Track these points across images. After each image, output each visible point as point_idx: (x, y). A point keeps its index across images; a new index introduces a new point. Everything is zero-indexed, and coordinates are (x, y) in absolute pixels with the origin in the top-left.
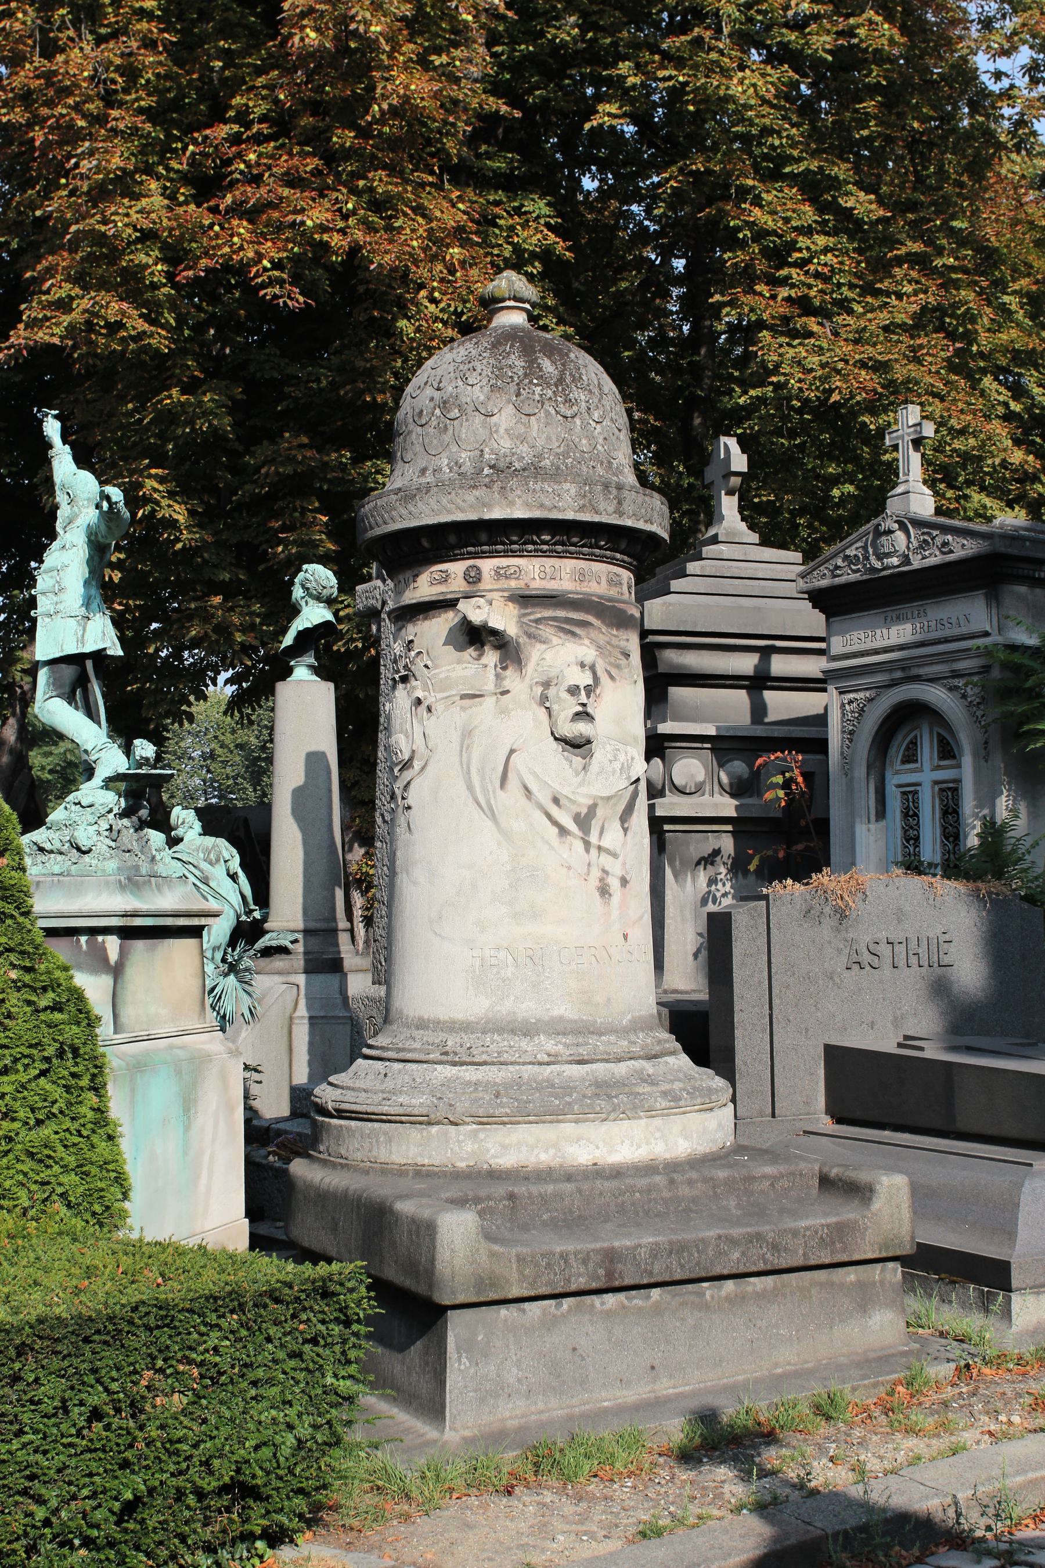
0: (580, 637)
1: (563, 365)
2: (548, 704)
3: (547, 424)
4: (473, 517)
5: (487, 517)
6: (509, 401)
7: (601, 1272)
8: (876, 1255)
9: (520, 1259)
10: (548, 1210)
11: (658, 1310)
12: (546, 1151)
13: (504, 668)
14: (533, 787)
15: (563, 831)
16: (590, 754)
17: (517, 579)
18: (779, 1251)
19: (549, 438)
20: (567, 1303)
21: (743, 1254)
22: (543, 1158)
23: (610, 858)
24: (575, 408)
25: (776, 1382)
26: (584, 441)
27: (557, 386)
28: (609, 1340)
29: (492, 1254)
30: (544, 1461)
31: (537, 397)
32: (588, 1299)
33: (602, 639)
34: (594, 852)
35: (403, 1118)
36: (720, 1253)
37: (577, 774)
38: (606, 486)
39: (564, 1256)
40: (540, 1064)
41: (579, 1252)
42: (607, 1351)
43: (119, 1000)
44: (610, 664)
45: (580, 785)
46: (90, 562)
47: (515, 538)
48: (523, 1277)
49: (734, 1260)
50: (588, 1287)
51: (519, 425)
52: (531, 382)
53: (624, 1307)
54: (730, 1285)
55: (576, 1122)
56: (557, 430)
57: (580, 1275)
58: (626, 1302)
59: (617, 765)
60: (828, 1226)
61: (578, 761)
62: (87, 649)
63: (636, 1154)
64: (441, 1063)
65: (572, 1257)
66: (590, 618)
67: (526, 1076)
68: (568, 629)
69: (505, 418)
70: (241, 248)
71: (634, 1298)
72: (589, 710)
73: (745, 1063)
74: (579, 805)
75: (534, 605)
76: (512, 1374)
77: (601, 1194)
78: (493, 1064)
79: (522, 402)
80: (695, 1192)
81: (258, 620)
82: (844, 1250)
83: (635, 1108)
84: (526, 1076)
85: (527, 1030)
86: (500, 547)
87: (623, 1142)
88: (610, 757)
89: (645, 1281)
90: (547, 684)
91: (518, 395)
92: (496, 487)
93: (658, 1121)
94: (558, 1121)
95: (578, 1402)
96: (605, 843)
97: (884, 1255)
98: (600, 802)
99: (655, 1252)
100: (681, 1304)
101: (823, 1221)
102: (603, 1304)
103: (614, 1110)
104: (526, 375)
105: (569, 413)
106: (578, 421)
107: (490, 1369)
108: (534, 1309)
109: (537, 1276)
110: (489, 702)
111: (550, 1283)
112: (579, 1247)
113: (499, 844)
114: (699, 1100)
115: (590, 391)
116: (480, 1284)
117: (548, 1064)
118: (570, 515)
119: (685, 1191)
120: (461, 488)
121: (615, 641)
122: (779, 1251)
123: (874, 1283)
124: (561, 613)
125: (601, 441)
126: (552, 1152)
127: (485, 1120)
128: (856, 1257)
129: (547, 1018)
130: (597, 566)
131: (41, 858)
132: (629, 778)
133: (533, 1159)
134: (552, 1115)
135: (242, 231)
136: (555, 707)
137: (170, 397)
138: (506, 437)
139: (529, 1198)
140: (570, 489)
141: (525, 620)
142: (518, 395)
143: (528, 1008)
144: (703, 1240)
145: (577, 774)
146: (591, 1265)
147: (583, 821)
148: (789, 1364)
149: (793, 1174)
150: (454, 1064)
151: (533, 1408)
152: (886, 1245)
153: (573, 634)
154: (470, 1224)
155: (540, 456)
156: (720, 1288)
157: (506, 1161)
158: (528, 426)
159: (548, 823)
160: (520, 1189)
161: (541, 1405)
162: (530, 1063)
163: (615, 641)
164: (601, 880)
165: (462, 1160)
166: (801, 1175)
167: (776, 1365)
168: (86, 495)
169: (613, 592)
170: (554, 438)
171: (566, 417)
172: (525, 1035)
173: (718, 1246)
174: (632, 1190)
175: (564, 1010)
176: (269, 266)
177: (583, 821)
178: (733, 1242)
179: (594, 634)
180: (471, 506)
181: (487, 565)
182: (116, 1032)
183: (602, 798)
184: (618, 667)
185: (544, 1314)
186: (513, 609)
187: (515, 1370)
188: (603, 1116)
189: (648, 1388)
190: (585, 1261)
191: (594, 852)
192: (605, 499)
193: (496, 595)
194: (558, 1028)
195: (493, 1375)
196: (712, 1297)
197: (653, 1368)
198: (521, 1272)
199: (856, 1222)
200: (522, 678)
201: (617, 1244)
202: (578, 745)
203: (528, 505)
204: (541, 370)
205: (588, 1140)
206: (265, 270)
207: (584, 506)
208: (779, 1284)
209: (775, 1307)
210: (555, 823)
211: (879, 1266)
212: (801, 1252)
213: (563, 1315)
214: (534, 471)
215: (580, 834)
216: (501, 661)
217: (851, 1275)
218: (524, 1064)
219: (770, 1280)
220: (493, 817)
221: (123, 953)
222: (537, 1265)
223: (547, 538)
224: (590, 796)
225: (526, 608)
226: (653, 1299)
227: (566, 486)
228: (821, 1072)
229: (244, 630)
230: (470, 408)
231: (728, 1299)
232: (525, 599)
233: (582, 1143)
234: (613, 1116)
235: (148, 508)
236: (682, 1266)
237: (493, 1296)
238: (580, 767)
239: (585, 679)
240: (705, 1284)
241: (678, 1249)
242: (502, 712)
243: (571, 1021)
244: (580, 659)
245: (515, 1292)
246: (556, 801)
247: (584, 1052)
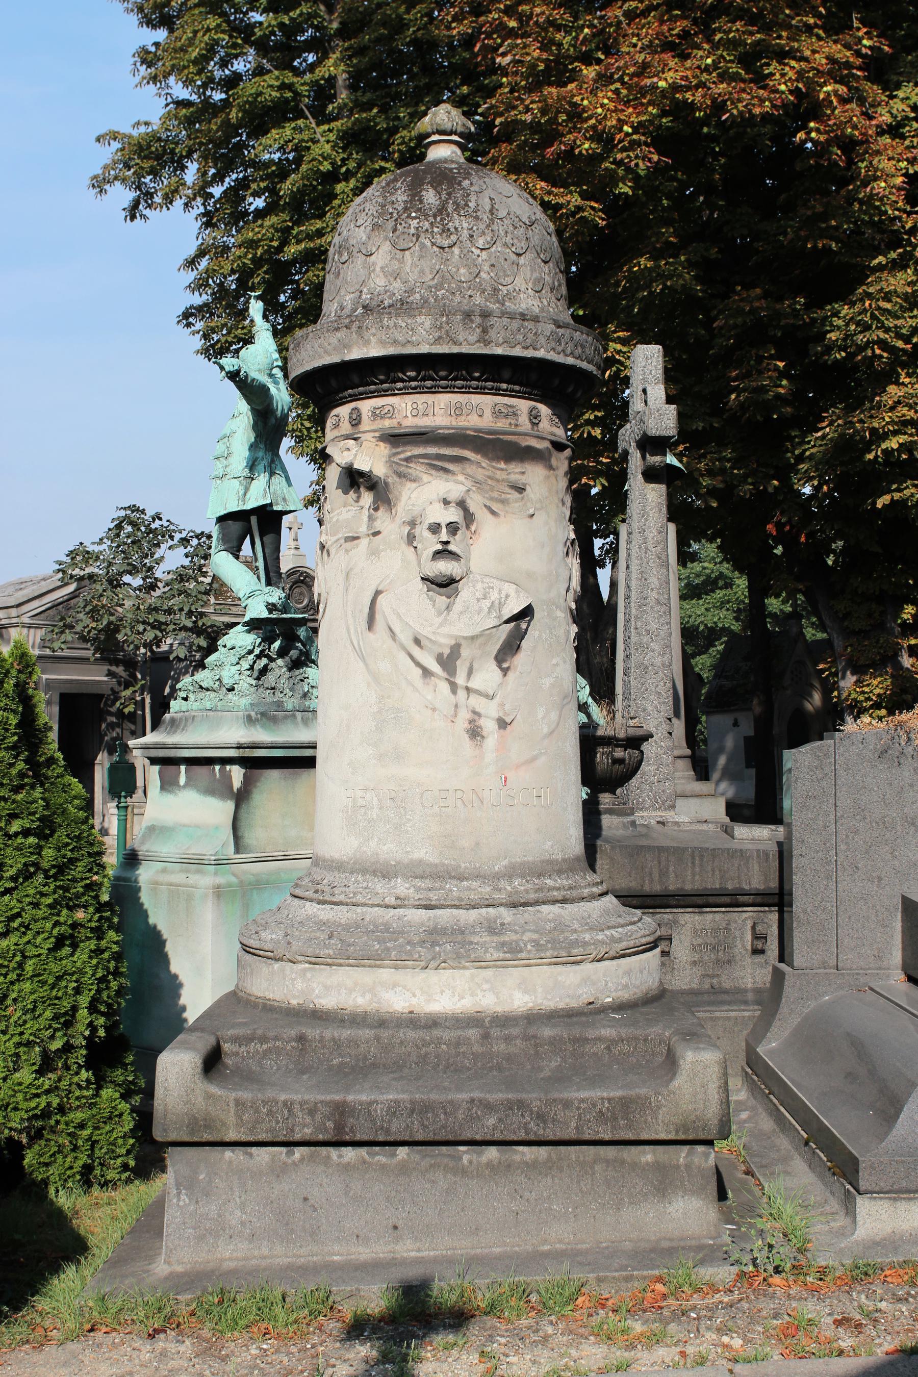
0: (453, 473)
1: (449, 194)
2: (415, 544)
3: (421, 257)
4: (336, 359)
5: (347, 358)
6: (386, 238)
7: (330, 1124)
8: (672, 1136)
9: (238, 1103)
10: (341, 1056)
11: (404, 1169)
12: (363, 995)
13: (376, 509)
14: (397, 629)
15: (427, 673)
16: (457, 592)
17: (390, 418)
18: (545, 1122)
19: (422, 272)
20: (299, 1152)
21: (500, 1120)
22: (359, 1001)
23: (483, 700)
24: (454, 238)
25: (473, 1261)
26: (462, 271)
27: (435, 217)
28: (346, 1194)
29: (209, 1096)
30: (215, 1306)
31: (412, 231)
32: (323, 1150)
33: (480, 474)
34: (462, 693)
35: (261, 953)
36: (472, 1118)
37: (440, 613)
38: (468, 315)
39: (288, 1105)
40: (387, 907)
41: (306, 1102)
42: (343, 1205)
43: (243, 824)
44: (492, 499)
45: (441, 625)
46: (255, 427)
47: (382, 377)
48: (240, 1123)
49: (489, 1126)
50: (314, 1138)
51: (394, 262)
52: (409, 216)
53: (364, 1162)
54: (492, 1153)
55: (396, 968)
56: (432, 262)
57: (305, 1126)
58: (367, 1157)
59: (486, 604)
60: (609, 1100)
61: (442, 600)
62: (249, 506)
63: (459, 1005)
64: (311, 900)
65: (297, 1106)
66: (467, 453)
67: (368, 918)
68: (439, 465)
69: (382, 257)
70: (605, 117)
71: (377, 1154)
72: (451, 547)
73: (805, 911)
74: (441, 645)
75: (405, 444)
76: (235, 1217)
77: (402, 1043)
78: (347, 904)
79: (398, 237)
80: (512, 1049)
81: (728, 465)
82: (630, 1127)
83: (458, 957)
84: (368, 918)
85: (385, 872)
86: (372, 387)
87: (442, 992)
88: (479, 595)
89: (381, 1139)
90: (412, 524)
91: (395, 230)
92: (354, 328)
93: (489, 973)
94: (379, 966)
95: (304, 1253)
96: (474, 684)
97: (682, 1137)
98: (463, 642)
99: (393, 1110)
100: (431, 1166)
101: (605, 1095)
102: (340, 1156)
103: (434, 958)
104: (406, 209)
105: (445, 243)
106: (456, 250)
107: (212, 1209)
108: (262, 1155)
109: (257, 1122)
110: (364, 542)
111: (271, 1130)
112: (306, 1097)
113: (369, 685)
114: (548, 954)
115: (477, 218)
116: (194, 1123)
117: (395, 907)
118: (425, 349)
119: (500, 1047)
120: (328, 331)
121: (499, 475)
122: (545, 1122)
123: (677, 1167)
124: (432, 450)
125: (486, 268)
126: (368, 996)
127: (313, 960)
128: (645, 1136)
129: (406, 861)
130: (476, 399)
131: (202, 695)
132: (499, 617)
133: (351, 1002)
134: (370, 959)
135: (606, 101)
136: (419, 546)
137: (639, 264)
138: (381, 274)
139: (320, 1041)
140: (425, 321)
141: (395, 459)
142: (395, 230)
143: (388, 849)
144: (451, 1102)
145: (440, 613)
146: (318, 1117)
147: (448, 662)
148: (560, 1241)
149: (636, 1039)
150: (320, 902)
151: (256, 1253)
152: (685, 1128)
153: (446, 471)
154: (186, 1065)
155: (410, 292)
156: (480, 1154)
157: (328, 1002)
158: (402, 261)
159: (412, 664)
160: (313, 1033)
161: (265, 1251)
162: (379, 906)
163: (499, 475)
164: (471, 722)
165: (294, 997)
166: (645, 1040)
167: (545, 1241)
168: (256, 367)
169: (502, 424)
170: (427, 270)
171: (443, 248)
172: (384, 877)
173: (470, 1110)
174: (439, 1041)
175: (424, 853)
176: (630, 130)
177: (448, 662)
178: (489, 1107)
179: (470, 469)
180: (335, 349)
181: (366, 406)
182: (237, 851)
183: (465, 638)
184: (503, 502)
185: (273, 1160)
186: (384, 449)
187: (238, 1213)
188: (423, 964)
189: (389, 1248)
190: (312, 1112)
191: (462, 693)
192: (466, 329)
193: (369, 436)
194: (416, 871)
195: (213, 1214)
196: (471, 1162)
197: (395, 1228)
198: (239, 1117)
199: (647, 1098)
200: (393, 518)
201: (350, 1098)
202: (446, 584)
203: (382, 343)
204: (421, 202)
205: (404, 987)
206: (627, 134)
207: (440, 338)
208: (554, 1156)
209: (549, 1181)
210: (418, 664)
211: (686, 1148)
212: (573, 1124)
213: (294, 1163)
214: (403, 307)
215: (445, 675)
216: (375, 502)
217: (648, 1155)
218: (373, 906)
219: (543, 1151)
220: (363, 659)
221: (248, 782)
222: (257, 1111)
223: (412, 374)
224: (451, 636)
225: (398, 447)
226: (399, 1157)
227: (420, 319)
228: (898, 925)
229: (710, 473)
230: (355, 250)
231: (489, 1165)
232: (395, 438)
233: (398, 989)
234: (433, 964)
235: (614, 369)
236: (425, 1127)
237: (207, 1137)
238: (444, 607)
239: (453, 515)
240: (462, 1148)
241: (422, 1109)
242: (373, 554)
243: (430, 865)
244: (442, 495)
245: (232, 1136)
246: (417, 642)
247: (434, 897)
